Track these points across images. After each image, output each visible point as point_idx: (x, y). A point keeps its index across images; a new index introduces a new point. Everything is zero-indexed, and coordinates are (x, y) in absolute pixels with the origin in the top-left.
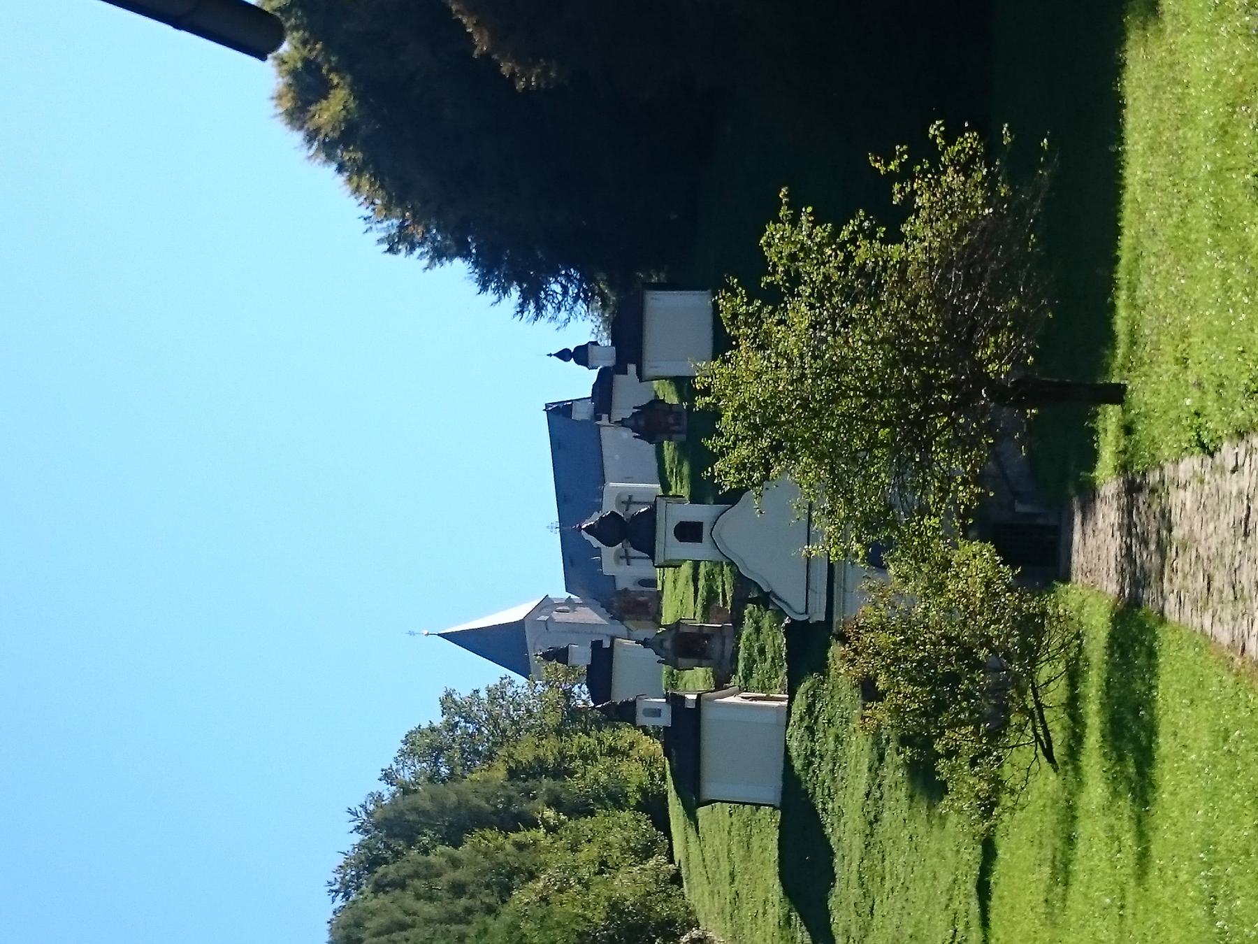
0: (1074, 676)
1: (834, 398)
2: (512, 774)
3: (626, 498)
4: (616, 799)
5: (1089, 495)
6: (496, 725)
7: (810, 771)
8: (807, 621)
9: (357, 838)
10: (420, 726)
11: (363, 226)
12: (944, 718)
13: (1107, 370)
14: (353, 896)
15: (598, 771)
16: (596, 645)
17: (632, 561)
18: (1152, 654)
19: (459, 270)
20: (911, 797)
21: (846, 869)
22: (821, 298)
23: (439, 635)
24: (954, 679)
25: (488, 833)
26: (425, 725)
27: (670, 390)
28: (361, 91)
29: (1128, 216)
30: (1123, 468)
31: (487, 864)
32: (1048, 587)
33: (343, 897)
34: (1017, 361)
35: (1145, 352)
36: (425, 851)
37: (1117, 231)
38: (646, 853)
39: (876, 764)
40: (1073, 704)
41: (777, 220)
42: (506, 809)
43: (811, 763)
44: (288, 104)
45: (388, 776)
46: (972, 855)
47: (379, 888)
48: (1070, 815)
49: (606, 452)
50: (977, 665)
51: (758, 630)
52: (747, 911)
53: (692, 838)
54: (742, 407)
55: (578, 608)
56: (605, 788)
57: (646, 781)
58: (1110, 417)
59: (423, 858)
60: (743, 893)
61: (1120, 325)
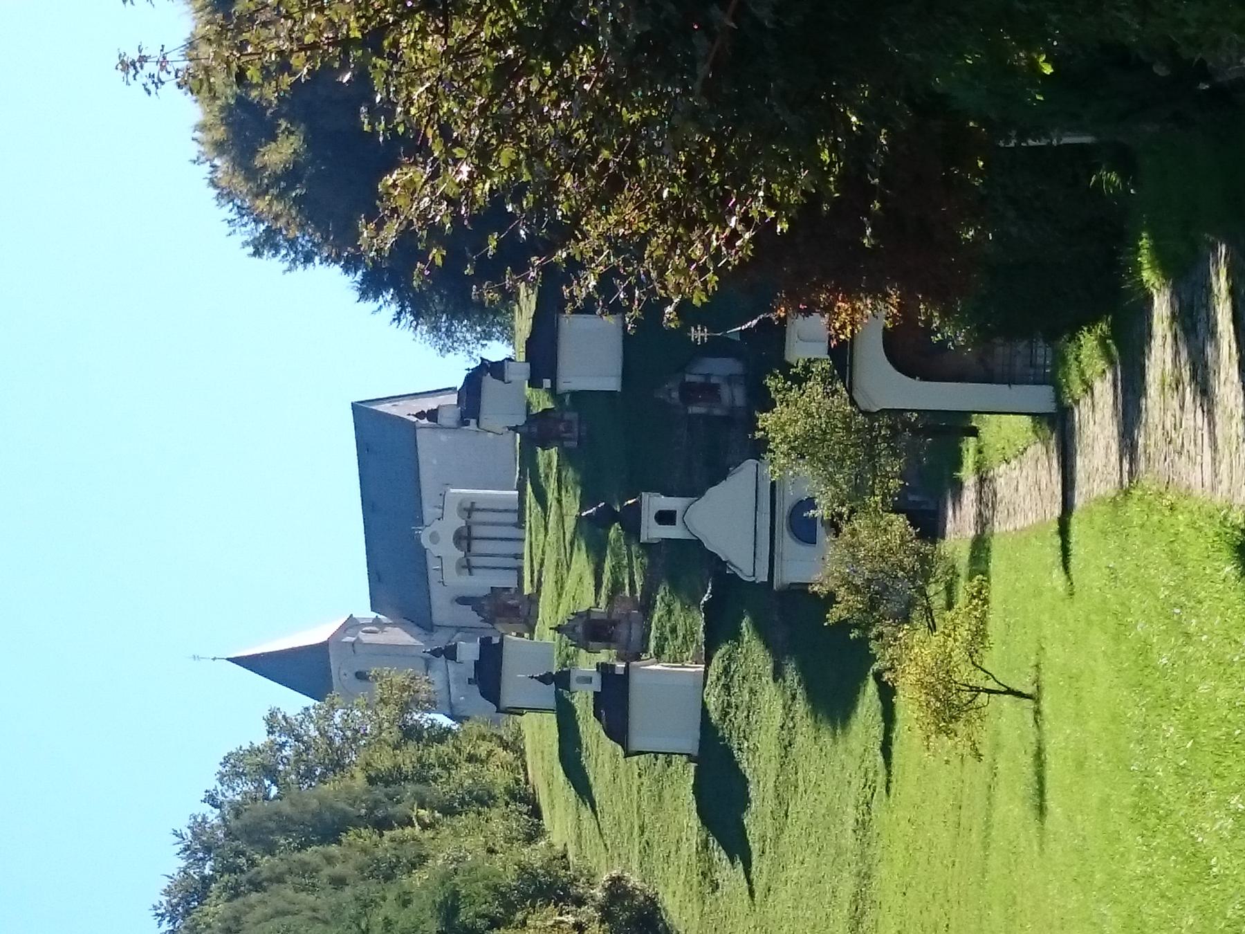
3: (468, 505)
4: (483, 799)
5: (958, 486)
7: (727, 720)
8: (754, 582)
10: (241, 747)
11: (227, 229)
15: (464, 773)
16: (485, 643)
17: (474, 571)
18: (989, 550)
23: (228, 659)
27: (546, 397)
33: (169, 921)
39: (790, 702)
43: (728, 713)
46: (878, 731)
49: (422, 456)
51: (670, 612)
55: (387, 629)
56: (470, 793)
57: (512, 784)
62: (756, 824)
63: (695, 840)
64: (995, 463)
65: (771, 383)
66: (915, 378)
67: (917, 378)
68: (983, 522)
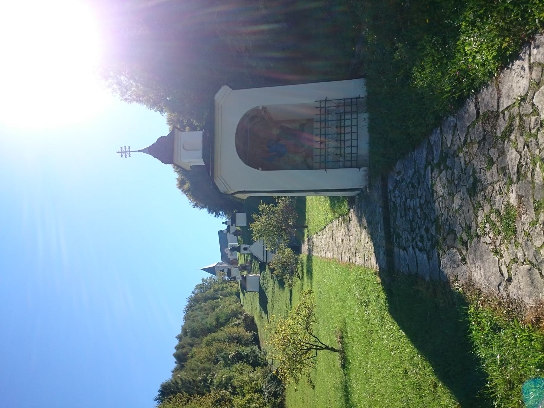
0: (302, 266)
1: (269, 228)
2: (214, 291)
4: (231, 294)
5: (303, 241)
6: (211, 283)
9: (188, 303)
11: (189, 203)
12: (285, 273)
13: (305, 224)
14: (187, 313)
15: (229, 290)
16: (228, 269)
18: (312, 260)
19: (205, 210)
20: (279, 288)
21: (269, 301)
22: (267, 215)
24: (286, 267)
25: (211, 301)
26: (199, 284)
28: (192, 183)
29: (307, 204)
30: (308, 237)
31: (211, 306)
32: (298, 255)
34: (293, 223)
35: (310, 221)
36: (200, 304)
37: (306, 205)
38: (237, 302)
40: (302, 271)
41: (261, 204)
42: (213, 296)
44: (179, 186)
45: (193, 293)
46: (289, 295)
47: (193, 311)
48: (302, 285)
50: (289, 265)
52: (254, 309)
53: (244, 299)
54: (257, 229)
57: (236, 291)
58: (306, 230)
59: (200, 305)
60: (253, 306)
61: (307, 218)
62: (269, 308)
63: (258, 309)
64: (313, 234)
65: (254, 216)
66: (258, 169)
67: (260, 168)
68: (310, 251)
